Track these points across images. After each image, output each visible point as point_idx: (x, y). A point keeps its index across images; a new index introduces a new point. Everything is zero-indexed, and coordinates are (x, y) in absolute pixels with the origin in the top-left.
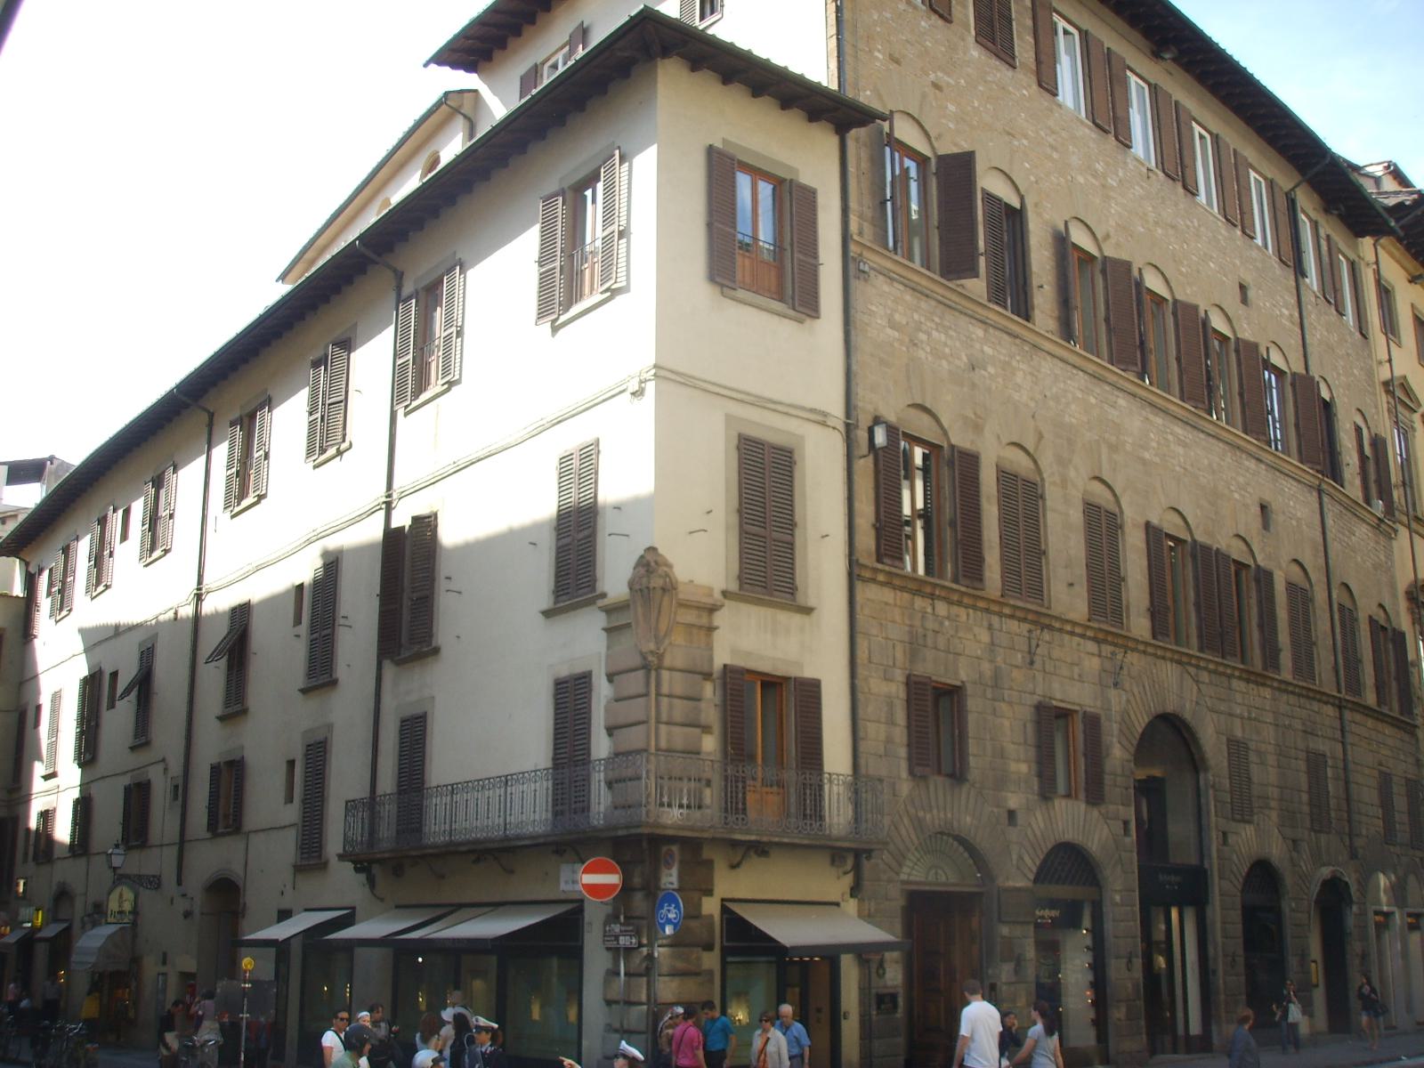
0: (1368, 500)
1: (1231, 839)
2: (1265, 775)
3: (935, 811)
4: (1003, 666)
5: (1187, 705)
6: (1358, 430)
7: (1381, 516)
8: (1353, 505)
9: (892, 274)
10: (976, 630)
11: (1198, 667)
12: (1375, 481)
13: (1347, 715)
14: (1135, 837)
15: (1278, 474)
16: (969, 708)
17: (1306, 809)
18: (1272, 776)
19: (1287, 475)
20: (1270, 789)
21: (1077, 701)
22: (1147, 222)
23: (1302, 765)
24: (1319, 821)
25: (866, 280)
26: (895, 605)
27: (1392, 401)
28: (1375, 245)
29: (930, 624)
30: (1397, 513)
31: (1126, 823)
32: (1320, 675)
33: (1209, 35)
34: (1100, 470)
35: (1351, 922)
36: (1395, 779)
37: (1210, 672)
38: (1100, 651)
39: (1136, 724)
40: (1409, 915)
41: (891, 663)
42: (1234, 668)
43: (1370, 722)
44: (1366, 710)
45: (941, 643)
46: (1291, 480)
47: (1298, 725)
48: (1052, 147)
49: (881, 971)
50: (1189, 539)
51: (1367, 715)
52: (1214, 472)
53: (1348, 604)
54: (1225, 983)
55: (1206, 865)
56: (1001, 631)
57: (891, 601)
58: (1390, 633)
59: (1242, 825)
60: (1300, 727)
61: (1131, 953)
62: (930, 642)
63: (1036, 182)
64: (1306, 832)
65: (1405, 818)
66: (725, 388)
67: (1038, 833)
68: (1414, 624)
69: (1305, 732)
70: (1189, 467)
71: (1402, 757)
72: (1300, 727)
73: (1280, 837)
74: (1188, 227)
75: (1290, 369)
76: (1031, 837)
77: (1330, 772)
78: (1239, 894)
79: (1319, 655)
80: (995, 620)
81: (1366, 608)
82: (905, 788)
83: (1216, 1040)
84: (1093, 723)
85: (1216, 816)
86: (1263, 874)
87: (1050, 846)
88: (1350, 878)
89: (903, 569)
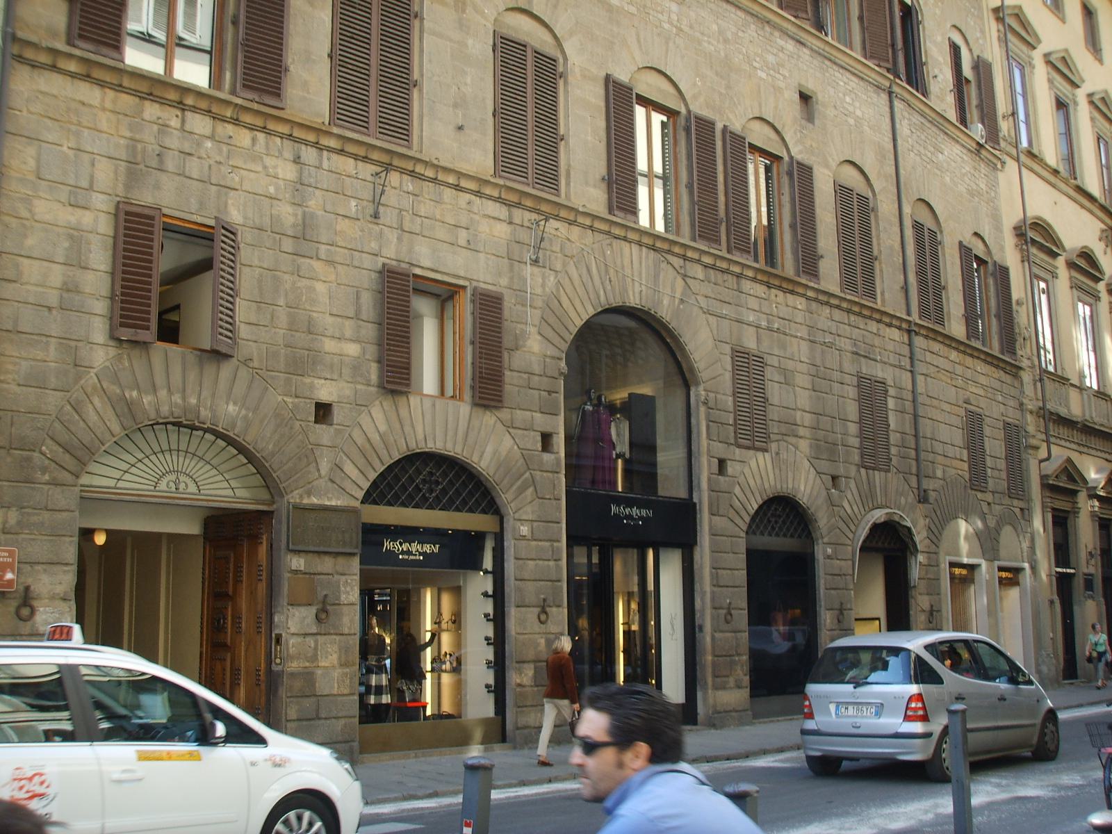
0: (963, 121)
1: (731, 468)
2: (790, 397)
3: (163, 393)
4: (321, 213)
5: (666, 302)
6: (955, 50)
7: (982, 141)
8: (941, 121)
10: (269, 161)
11: (685, 258)
12: (977, 106)
13: (919, 342)
14: (563, 455)
15: (827, 62)
17: (855, 442)
18: (804, 399)
19: (842, 67)
20: (799, 413)
21: (462, 274)
23: (852, 392)
24: (874, 451)
26: (104, 109)
27: (1001, 28)
29: (173, 141)
30: (1003, 144)
31: (546, 439)
32: (883, 294)
35: (915, 573)
36: (987, 420)
37: (808, 299)
38: (510, 216)
39: (573, 314)
40: (1001, 569)
41: (85, 184)
42: (743, 266)
43: (954, 355)
44: (949, 341)
46: (848, 75)
47: (846, 345)
49: (25, 612)
50: (683, 111)
51: (949, 346)
52: (726, 41)
53: (929, 223)
54: (713, 638)
55: (695, 500)
56: (318, 167)
57: (96, 102)
58: (990, 266)
59: (752, 452)
60: (849, 348)
61: (544, 600)
62: (170, 165)
64: (853, 469)
65: (1002, 464)
66: (1024, 275)
67: (375, 438)
68: (1023, 261)
69: (853, 353)
70: (686, 29)
71: (1000, 398)
72: (849, 348)
76: (360, 440)
77: (891, 403)
78: (743, 535)
79: (881, 271)
80: (309, 154)
81: (954, 234)
82: (101, 355)
83: (701, 709)
84: (489, 307)
85: (709, 437)
86: (782, 511)
87: (397, 456)
88: (917, 524)
89: (637, 222)
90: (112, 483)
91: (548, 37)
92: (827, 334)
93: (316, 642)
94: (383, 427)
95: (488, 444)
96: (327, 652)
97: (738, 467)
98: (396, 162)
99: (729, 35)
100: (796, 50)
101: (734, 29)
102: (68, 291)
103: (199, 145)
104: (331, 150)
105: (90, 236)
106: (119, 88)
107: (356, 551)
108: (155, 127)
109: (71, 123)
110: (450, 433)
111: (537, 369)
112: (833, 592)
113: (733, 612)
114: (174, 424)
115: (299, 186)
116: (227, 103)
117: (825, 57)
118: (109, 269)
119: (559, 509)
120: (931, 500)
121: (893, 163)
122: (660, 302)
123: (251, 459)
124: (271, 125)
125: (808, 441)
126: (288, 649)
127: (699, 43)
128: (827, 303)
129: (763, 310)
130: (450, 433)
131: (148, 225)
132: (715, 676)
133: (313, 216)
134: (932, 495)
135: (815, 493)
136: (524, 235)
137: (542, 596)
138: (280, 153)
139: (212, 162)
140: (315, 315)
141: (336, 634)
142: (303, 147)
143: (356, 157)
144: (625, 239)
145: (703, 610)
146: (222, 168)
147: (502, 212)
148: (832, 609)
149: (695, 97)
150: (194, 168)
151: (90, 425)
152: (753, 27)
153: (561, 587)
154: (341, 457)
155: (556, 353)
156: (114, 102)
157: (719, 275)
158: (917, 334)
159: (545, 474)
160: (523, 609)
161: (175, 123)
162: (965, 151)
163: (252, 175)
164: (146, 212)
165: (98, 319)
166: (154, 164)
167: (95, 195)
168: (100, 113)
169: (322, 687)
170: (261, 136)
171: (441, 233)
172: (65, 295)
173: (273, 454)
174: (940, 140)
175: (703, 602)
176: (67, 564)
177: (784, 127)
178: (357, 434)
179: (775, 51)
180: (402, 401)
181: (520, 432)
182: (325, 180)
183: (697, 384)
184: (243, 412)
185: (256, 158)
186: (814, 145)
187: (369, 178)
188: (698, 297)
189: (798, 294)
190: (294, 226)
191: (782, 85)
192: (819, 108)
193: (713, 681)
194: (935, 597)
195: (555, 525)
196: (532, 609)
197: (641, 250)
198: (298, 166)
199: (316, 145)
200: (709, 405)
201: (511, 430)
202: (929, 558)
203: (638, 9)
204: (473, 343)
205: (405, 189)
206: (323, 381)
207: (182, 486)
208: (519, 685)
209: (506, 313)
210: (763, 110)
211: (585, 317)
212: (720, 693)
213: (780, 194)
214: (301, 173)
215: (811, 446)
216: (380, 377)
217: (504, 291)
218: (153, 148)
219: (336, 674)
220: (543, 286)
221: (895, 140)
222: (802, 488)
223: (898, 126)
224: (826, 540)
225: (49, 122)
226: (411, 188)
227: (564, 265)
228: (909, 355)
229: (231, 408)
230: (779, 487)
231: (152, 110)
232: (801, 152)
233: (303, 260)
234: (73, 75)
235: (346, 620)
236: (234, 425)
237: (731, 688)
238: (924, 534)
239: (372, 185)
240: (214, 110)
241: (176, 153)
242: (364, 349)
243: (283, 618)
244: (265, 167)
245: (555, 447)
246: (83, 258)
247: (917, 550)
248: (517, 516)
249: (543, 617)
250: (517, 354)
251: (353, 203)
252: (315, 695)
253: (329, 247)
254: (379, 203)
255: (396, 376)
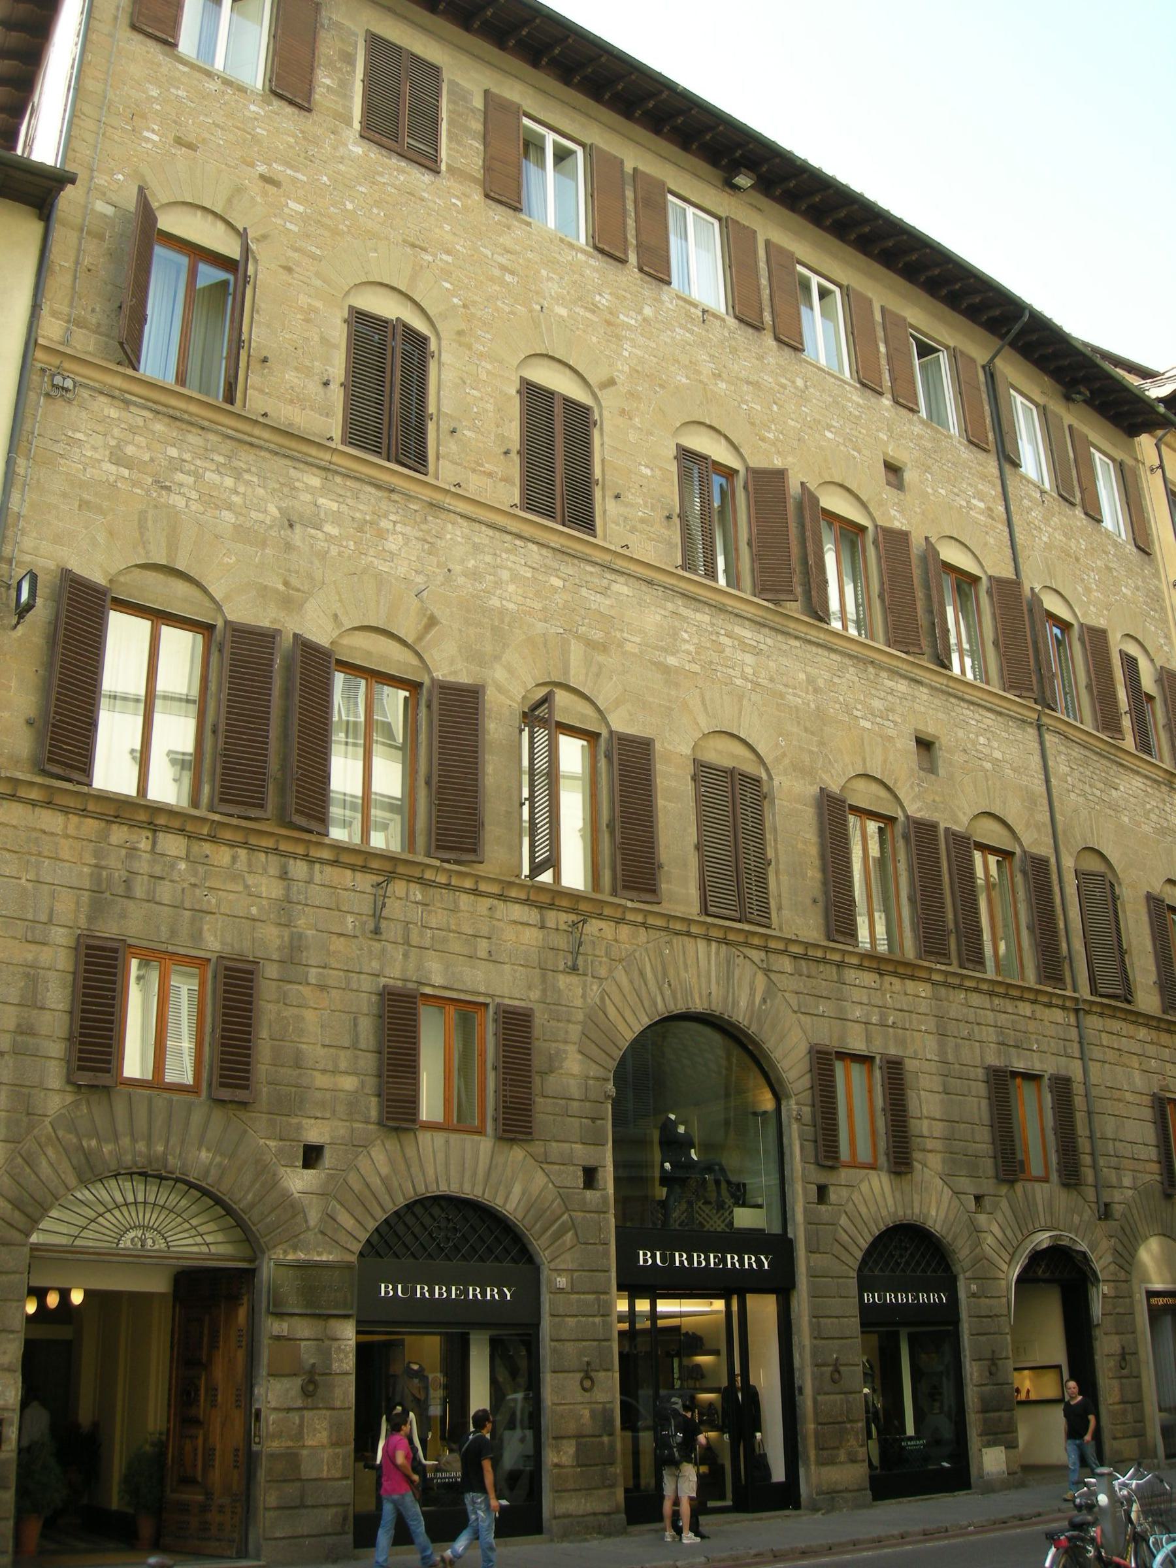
3: (126, 1141)
8: (1113, 751)
9: (127, 396)
10: (250, 880)
11: (766, 949)
13: (1093, 1022)
14: (611, 1190)
15: (953, 700)
16: (984, 1103)
19: (973, 703)
21: (482, 989)
22: (699, 373)
25: (70, 401)
26: (67, 836)
28: (1157, 445)
31: (590, 1176)
33: (872, 199)
34: (566, 671)
35: (1097, 1309)
37: (934, 984)
38: (543, 920)
39: (622, 1027)
41: (44, 918)
43: (1142, 1033)
45: (165, 892)
47: (990, 1035)
48: (504, 268)
52: (817, 690)
54: (815, 1402)
55: (790, 1235)
57: (59, 830)
61: (588, 1364)
62: (139, 891)
63: (465, 306)
67: (375, 1182)
70: (765, 682)
72: (993, 1038)
73: (947, 1192)
74: (783, 387)
75: (985, 572)
76: (357, 1186)
90: (64, 1241)
91: (588, 710)
92: (961, 1024)
93: (302, 1418)
94: (385, 1170)
95: (513, 1183)
96: (315, 1429)
97: (844, 1193)
98: (401, 869)
99: (821, 683)
100: (910, 691)
101: (827, 676)
102: (22, 1033)
103: (172, 866)
104: (322, 862)
105: (49, 973)
106: (84, 813)
107: (350, 1312)
108: (124, 852)
109: (31, 854)
110: (468, 1174)
111: (575, 1091)
112: (980, 1338)
113: (842, 1369)
114: (140, 1174)
115: (285, 904)
116: (204, 820)
117: (950, 695)
118: (67, 1008)
119: (606, 1254)
120: (1117, 1215)
121: (1047, 808)
122: (735, 1003)
123: (229, 1211)
124: (253, 841)
125: (939, 1156)
126: (267, 1426)
127: (782, 696)
128: (960, 987)
129: (873, 1002)
130: (468, 1174)
131: (87, 1019)
132: (820, 1448)
133: (300, 936)
134: (1118, 1210)
135: (951, 1217)
136: (561, 941)
137: (586, 1359)
138: (265, 869)
139: (185, 885)
140: (304, 1046)
141: (327, 1409)
142: (291, 861)
143: (353, 868)
144: (688, 934)
145: (802, 1368)
146: (197, 891)
147: (533, 916)
148: (980, 1360)
149: (778, 760)
150: (165, 892)
151: (43, 1179)
152: (851, 670)
153: (611, 1347)
154: (334, 1206)
155: (601, 1073)
156: (78, 828)
157: (813, 965)
158: (1087, 1012)
159: (588, 1215)
160: (560, 1375)
161: (144, 845)
162: (1149, 783)
163: (232, 896)
164: (109, 944)
165: (54, 1062)
166: (121, 891)
167: (54, 929)
168: (63, 841)
169: (308, 1470)
170: (242, 853)
171: (456, 946)
172: (19, 1038)
173: (252, 1205)
174: (1112, 772)
175: (803, 1359)
176: (12, 1332)
177: (895, 783)
178: (353, 1179)
179: (883, 694)
180: (408, 1139)
181: (557, 1167)
182: (318, 895)
183: (788, 1097)
184: (218, 1159)
185: (236, 877)
186: (937, 799)
187: (369, 889)
188: (787, 995)
189: (920, 979)
190: (279, 949)
191: (892, 733)
192: (942, 755)
193: (817, 1455)
194: (1130, 1336)
195: (601, 1274)
196: (571, 1375)
197: (709, 945)
198: (285, 883)
199: (306, 857)
200: (803, 1121)
201: (544, 1166)
202: (1116, 1288)
203: (703, 667)
204: (495, 1068)
205: (412, 898)
206: (313, 1121)
207: (150, 1242)
208: (557, 1465)
209: (537, 1032)
210: (868, 764)
211: (638, 1029)
212: (825, 1470)
213: (895, 861)
214: (288, 889)
215: (944, 1161)
216: (380, 1113)
217: (535, 1006)
218: (119, 875)
219: (326, 1454)
220: (584, 996)
221: (1047, 781)
222: (933, 1213)
223: (1050, 763)
224: (968, 1274)
225: (7, 855)
226: (419, 897)
227: (611, 971)
228: (1077, 1039)
229: (204, 1155)
230: (901, 1213)
231: (119, 834)
232: (920, 810)
233: (290, 986)
234: (34, 804)
235: (338, 1392)
236: (207, 1172)
237: (841, 1463)
238: (1108, 1258)
239: (372, 897)
240: (188, 829)
241: (146, 878)
242: (363, 1083)
243: (262, 1391)
244: (247, 887)
245: (601, 1182)
246: (39, 997)
247: (1098, 1280)
248: (552, 1265)
249: (587, 1384)
250: (551, 1078)
251: (350, 919)
252: (300, 1480)
253: (320, 970)
254: (380, 917)
255: (398, 1113)
